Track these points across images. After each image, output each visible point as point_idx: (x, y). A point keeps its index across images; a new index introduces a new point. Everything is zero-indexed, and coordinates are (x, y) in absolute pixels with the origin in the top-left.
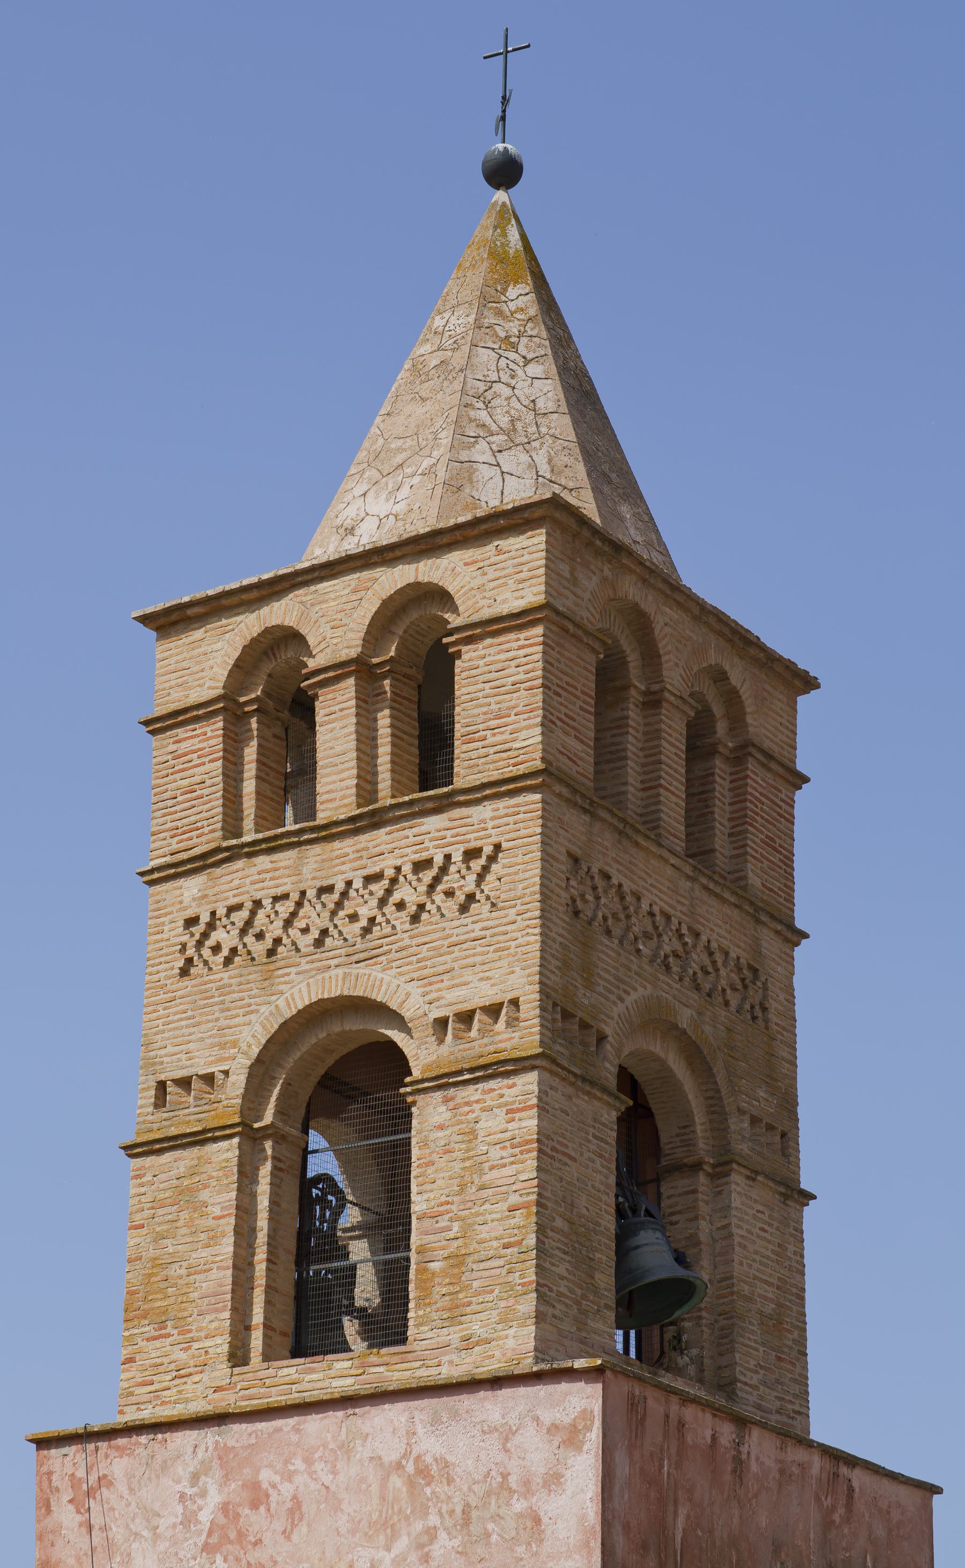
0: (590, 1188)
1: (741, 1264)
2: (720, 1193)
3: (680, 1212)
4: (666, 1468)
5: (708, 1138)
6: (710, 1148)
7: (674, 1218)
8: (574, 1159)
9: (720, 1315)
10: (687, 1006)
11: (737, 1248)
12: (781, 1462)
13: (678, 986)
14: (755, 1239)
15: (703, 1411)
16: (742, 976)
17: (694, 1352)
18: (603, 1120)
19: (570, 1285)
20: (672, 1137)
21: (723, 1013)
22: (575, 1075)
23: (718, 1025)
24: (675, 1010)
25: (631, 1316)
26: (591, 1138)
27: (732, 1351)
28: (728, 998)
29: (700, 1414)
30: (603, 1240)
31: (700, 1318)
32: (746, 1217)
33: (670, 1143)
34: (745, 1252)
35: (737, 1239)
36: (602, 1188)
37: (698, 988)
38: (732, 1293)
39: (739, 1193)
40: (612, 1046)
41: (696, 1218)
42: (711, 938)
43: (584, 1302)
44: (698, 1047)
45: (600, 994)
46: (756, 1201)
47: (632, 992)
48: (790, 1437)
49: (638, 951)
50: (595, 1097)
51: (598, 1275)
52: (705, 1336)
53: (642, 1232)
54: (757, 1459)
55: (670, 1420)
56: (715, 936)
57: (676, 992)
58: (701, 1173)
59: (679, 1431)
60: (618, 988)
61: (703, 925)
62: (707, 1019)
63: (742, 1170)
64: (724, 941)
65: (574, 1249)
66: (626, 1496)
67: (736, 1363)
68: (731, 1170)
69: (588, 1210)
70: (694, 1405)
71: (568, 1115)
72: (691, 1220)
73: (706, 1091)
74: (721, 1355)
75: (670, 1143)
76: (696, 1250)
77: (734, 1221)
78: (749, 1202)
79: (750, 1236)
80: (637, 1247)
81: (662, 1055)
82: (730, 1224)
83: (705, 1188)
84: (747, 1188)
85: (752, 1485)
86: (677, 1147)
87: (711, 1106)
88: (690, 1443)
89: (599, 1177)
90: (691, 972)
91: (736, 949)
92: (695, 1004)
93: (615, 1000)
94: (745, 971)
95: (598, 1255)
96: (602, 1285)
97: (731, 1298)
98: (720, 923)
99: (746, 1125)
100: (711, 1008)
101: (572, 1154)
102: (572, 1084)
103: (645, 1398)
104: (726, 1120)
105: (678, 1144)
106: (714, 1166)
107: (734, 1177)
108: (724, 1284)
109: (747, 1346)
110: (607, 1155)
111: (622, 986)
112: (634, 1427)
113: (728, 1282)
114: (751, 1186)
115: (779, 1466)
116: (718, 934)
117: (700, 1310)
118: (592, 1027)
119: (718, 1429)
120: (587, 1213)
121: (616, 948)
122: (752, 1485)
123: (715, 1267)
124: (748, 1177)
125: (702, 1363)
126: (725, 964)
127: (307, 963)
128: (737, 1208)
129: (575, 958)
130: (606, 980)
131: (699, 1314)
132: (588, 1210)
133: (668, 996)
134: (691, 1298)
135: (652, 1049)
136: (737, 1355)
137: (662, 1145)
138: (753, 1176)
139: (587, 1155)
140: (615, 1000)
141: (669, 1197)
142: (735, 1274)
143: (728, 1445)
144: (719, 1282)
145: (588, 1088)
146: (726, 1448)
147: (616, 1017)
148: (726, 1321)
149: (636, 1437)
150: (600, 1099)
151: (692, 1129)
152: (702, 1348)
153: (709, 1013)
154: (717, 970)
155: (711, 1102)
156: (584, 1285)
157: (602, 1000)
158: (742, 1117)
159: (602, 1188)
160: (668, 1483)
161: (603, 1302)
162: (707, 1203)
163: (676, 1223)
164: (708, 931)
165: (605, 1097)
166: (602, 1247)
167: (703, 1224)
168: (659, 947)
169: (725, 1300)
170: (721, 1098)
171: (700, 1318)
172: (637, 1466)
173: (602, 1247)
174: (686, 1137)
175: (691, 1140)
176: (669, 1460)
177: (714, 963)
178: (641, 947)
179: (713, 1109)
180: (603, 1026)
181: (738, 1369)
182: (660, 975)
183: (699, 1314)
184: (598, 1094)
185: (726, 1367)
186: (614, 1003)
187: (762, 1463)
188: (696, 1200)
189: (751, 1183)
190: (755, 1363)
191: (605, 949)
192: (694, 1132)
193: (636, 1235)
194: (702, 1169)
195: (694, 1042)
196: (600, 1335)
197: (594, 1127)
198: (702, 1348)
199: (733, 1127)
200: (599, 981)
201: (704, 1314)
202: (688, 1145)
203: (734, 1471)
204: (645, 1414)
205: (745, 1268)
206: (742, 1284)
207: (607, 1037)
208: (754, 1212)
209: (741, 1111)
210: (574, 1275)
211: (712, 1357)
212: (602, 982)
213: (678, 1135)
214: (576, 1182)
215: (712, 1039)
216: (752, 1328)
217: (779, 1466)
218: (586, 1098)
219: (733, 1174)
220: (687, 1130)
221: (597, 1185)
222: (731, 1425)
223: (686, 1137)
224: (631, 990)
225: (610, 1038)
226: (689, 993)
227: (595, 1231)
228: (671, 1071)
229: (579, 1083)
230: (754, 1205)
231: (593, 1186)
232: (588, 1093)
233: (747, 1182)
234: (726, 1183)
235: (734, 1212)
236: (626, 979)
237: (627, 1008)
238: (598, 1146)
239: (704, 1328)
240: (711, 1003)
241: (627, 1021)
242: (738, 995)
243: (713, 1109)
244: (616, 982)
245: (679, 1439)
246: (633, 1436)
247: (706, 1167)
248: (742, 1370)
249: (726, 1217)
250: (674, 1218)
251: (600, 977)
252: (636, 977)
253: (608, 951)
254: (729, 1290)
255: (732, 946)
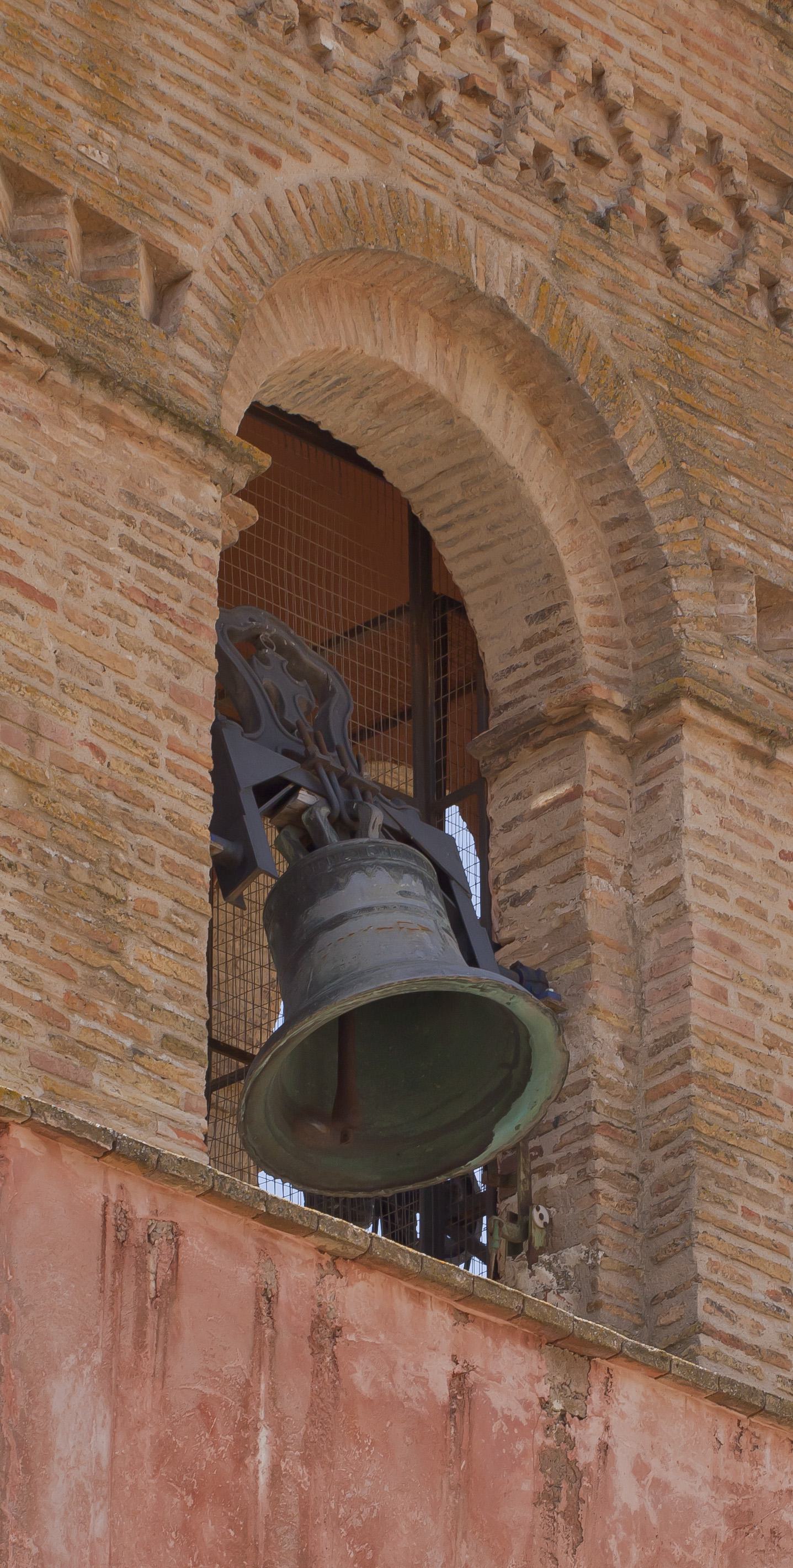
0: (108, 691)
1: (720, 995)
2: (653, 796)
3: (536, 863)
4: (264, 1456)
5: (619, 645)
6: (629, 674)
7: (521, 885)
8: (48, 603)
9: (655, 1147)
10: (510, 237)
11: (701, 949)
12: (733, 1488)
13: (476, 175)
14: (775, 933)
15: (417, 1298)
16: (731, 191)
17: (572, 1255)
18: (165, 504)
19: (22, 961)
20: (513, 652)
21: (653, 279)
22: (41, 349)
23: (633, 311)
24: (460, 238)
25: (344, 1138)
26: (114, 548)
27: (686, 1244)
28: (674, 238)
29: (403, 1306)
30: (160, 849)
31: (588, 1154)
32: (738, 866)
33: (513, 669)
34: (734, 965)
35: (700, 923)
36: (160, 699)
37: (557, 196)
38: (687, 1078)
39: (711, 793)
40: (203, 296)
41: (578, 870)
42: (607, 65)
43: (78, 1020)
44: (553, 359)
45: (160, 146)
46: (775, 824)
47: (288, 162)
48: (761, 1411)
49: (322, 55)
50: (132, 432)
51: (133, 949)
52: (603, 1208)
53: (357, 880)
54: (640, 1470)
55: (281, 1310)
56: (623, 59)
57: (464, 190)
58: (590, 739)
59: (317, 1348)
60: (235, 141)
61: (577, 23)
62: (590, 285)
63: (716, 722)
64: (658, 80)
65: (44, 859)
66: (99, 1525)
67: (697, 1279)
68: (682, 721)
69: (98, 752)
70: (376, 1277)
71: (22, 468)
72: (564, 879)
73: (604, 502)
74: (658, 1262)
75: (513, 669)
76: (577, 963)
77: (690, 869)
78: (752, 824)
79: (755, 922)
80: (341, 919)
81: (439, 384)
82: (679, 880)
83: (610, 786)
84: (742, 783)
85: (623, 1547)
86: (527, 681)
87: (623, 547)
88: (365, 1389)
89: (144, 665)
90: (527, 145)
91: (704, 109)
92: (542, 237)
93: (221, 170)
94: (739, 177)
95: (135, 891)
96: (157, 981)
97: (682, 1092)
98: (643, 27)
99: (743, 608)
100: (603, 257)
101: (39, 583)
102: (40, 380)
103: (176, 1232)
104: (666, 581)
105: (532, 668)
106: (630, 716)
107: (690, 742)
108: (664, 1055)
109: (737, 1232)
110: (180, 608)
111: (248, 137)
112: (128, 1315)
113: (675, 1048)
114: (763, 783)
115: (729, 1500)
116: (633, 57)
117: (588, 1130)
118: (126, 234)
119: (477, 1361)
120: (96, 764)
121: (227, 27)
122: (623, 1547)
123: (642, 1011)
124: (745, 752)
125: (594, 1285)
126: (664, 147)
127: (666, 1157)
128: (702, 835)
129: (58, 28)
130: (181, 108)
131: (584, 1144)
132: (98, 752)
133: (431, 195)
134: (527, 1076)
135: (399, 359)
136: (702, 1258)
137: (489, 682)
138: (762, 746)
139: (95, 594)
140: (221, 170)
141: (507, 828)
142: (694, 1021)
143: (523, 1416)
144: (652, 1055)
145: (96, 396)
146: (513, 1423)
147: (224, 222)
148: (671, 1163)
149: (139, 1345)
150: (152, 440)
151: (563, 614)
152: (595, 1241)
153: (596, 270)
154: (635, 159)
155: (620, 535)
156: (79, 970)
157: (169, 164)
158: (730, 586)
159: (160, 699)
160: (274, 1501)
161: (155, 1030)
162: (616, 829)
163: (528, 896)
164: (594, 42)
165: (166, 432)
166: (158, 871)
167: (597, 886)
168: (405, 52)
169: (670, 1099)
170: (644, 519)
171: (588, 1154)
172: (146, 1435)
173: (158, 871)
174: (551, 644)
175: (562, 648)
176: (278, 1431)
177: (623, 136)
178: (328, 42)
179: (627, 556)
180: (170, 237)
181: (703, 1295)
182: (399, 131)
183: (584, 1144)
184: (140, 420)
185: (671, 1295)
186: (216, 180)
187: (660, 1487)
188: (578, 818)
189: (759, 771)
190: (775, 1286)
191: (177, 19)
192: (568, 623)
193: (338, 887)
194: (590, 726)
195: (535, 341)
196: (140, 1124)
197: (129, 521)
198: (595, 1241)
199: (688, 605)
200: (157, 108)
201: (600, 1142)
202: (556, 667)
203: (548, 1497)
204: (175, 1278)
205: (735, 1008)
206: (719, 1052)
207: (188, 274)
208: (774, 856)
209: (718, 565)
210: (41, 936)
211: (629, 1271)
212: (167, 115)
213: (528, 644)
214: (51, 666)
215: (608, 344)
216: (760, 1184)
217: (729, 1500)
218: (96, 429)
219: (687, 736)
220: (551, 623)
221: (137, 686)
222: (533, 1355)
223: (551, 644)
224: (283, 155)
225: (199, 278)
226: (517, 200)
227: (125, 816)
228: (477, 437)
229: (62, 376)
230: (771, 836)
231: (122, 690)
232: (105, 418)
233: (746, 767)
234: (670, 764)
235: (689, 844)
236: (264, 119)
237: (268, 204)
238: (143, 577)
239: (600, 1184)
240: (606, 245)
241: (268, 238)
242: (714, 243)
243: (627, 556)
244: (223, 122)
245: (316, 1374)
246: (127, 1341)
247: (603, 719)
248: (720, 1300)
249: (668, 862)
250: (521, 885)
251: (161, 97)
252: (306, 122)
253: (189, 28)
254: (677, 1071)
255: (688, 100)
